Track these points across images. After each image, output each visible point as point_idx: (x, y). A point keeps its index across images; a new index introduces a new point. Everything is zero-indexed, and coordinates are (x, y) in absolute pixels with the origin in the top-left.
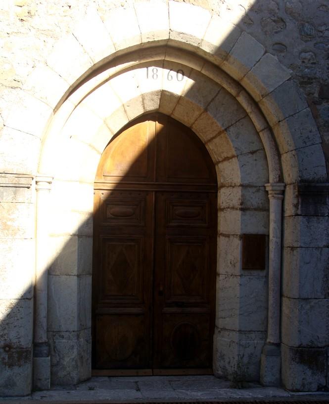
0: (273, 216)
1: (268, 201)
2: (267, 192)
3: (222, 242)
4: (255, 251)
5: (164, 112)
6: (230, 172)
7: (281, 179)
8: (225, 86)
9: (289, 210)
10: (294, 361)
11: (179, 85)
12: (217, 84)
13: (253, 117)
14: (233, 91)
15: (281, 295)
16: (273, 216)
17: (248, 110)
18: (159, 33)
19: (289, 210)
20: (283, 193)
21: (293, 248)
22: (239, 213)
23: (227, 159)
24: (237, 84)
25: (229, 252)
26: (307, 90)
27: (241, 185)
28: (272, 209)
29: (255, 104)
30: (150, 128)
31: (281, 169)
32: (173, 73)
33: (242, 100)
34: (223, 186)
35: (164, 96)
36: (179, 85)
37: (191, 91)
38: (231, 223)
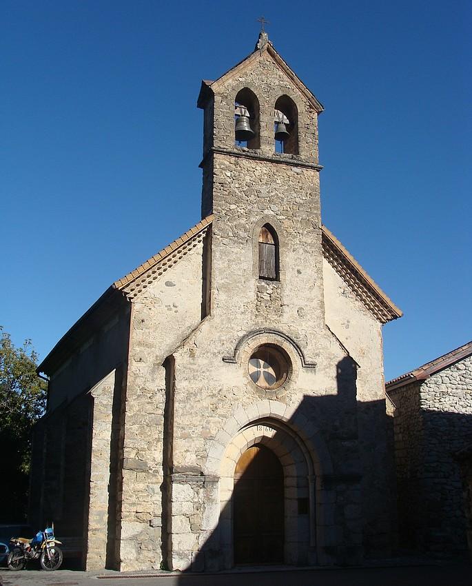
0: (311, 490)
1: (308, 483)
2: (307, 479)
3: (287, 502)
4: (303, 505)
5: (262, 444)
6: (291, 471)
7: (314, 474)
8: (290, 433)
9: (318, 487)
10: (289, 219)
11: (270, 433)
12: (286, 433)
13: (302, 447)
14: (294, 436)
15: (316, 525)
16: (311, 490)
17: (300, 444)
18: (254, 415)
19: (318, 487)
20: (315, 480)
21: (320, 504)
22: (296, 489)
23: (290, 465)
24: (295, 433)
25: (291, 507)
26: (266, 212)
27: (297, 477)
28: (310, 486)
29: (302, 441)
30: (255, 449)
31: (315, 508)
32: (268, 428)
33: (296, 439)
34: (287, 477)
35: (264, 437)
36: (270, 433)
37: (275, 436)
38: (292, 493)
